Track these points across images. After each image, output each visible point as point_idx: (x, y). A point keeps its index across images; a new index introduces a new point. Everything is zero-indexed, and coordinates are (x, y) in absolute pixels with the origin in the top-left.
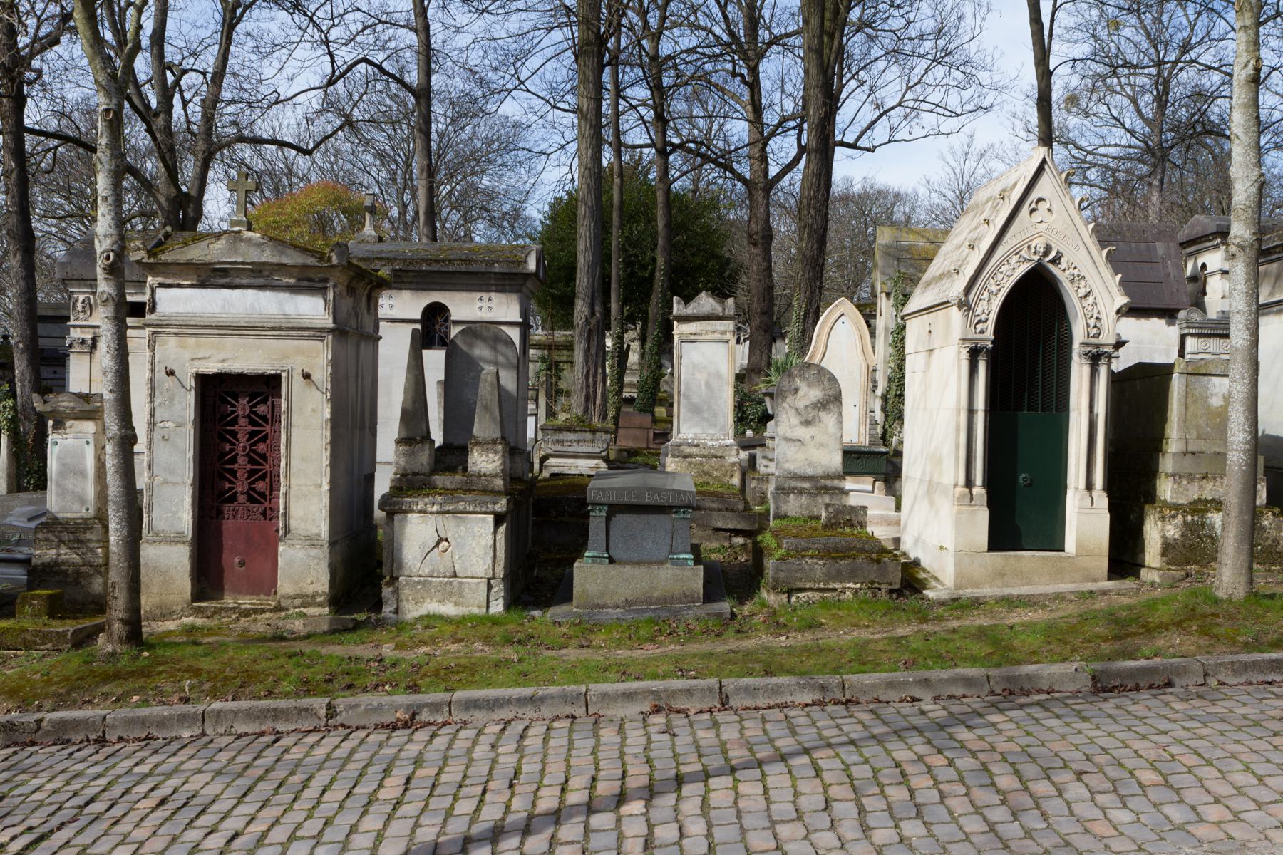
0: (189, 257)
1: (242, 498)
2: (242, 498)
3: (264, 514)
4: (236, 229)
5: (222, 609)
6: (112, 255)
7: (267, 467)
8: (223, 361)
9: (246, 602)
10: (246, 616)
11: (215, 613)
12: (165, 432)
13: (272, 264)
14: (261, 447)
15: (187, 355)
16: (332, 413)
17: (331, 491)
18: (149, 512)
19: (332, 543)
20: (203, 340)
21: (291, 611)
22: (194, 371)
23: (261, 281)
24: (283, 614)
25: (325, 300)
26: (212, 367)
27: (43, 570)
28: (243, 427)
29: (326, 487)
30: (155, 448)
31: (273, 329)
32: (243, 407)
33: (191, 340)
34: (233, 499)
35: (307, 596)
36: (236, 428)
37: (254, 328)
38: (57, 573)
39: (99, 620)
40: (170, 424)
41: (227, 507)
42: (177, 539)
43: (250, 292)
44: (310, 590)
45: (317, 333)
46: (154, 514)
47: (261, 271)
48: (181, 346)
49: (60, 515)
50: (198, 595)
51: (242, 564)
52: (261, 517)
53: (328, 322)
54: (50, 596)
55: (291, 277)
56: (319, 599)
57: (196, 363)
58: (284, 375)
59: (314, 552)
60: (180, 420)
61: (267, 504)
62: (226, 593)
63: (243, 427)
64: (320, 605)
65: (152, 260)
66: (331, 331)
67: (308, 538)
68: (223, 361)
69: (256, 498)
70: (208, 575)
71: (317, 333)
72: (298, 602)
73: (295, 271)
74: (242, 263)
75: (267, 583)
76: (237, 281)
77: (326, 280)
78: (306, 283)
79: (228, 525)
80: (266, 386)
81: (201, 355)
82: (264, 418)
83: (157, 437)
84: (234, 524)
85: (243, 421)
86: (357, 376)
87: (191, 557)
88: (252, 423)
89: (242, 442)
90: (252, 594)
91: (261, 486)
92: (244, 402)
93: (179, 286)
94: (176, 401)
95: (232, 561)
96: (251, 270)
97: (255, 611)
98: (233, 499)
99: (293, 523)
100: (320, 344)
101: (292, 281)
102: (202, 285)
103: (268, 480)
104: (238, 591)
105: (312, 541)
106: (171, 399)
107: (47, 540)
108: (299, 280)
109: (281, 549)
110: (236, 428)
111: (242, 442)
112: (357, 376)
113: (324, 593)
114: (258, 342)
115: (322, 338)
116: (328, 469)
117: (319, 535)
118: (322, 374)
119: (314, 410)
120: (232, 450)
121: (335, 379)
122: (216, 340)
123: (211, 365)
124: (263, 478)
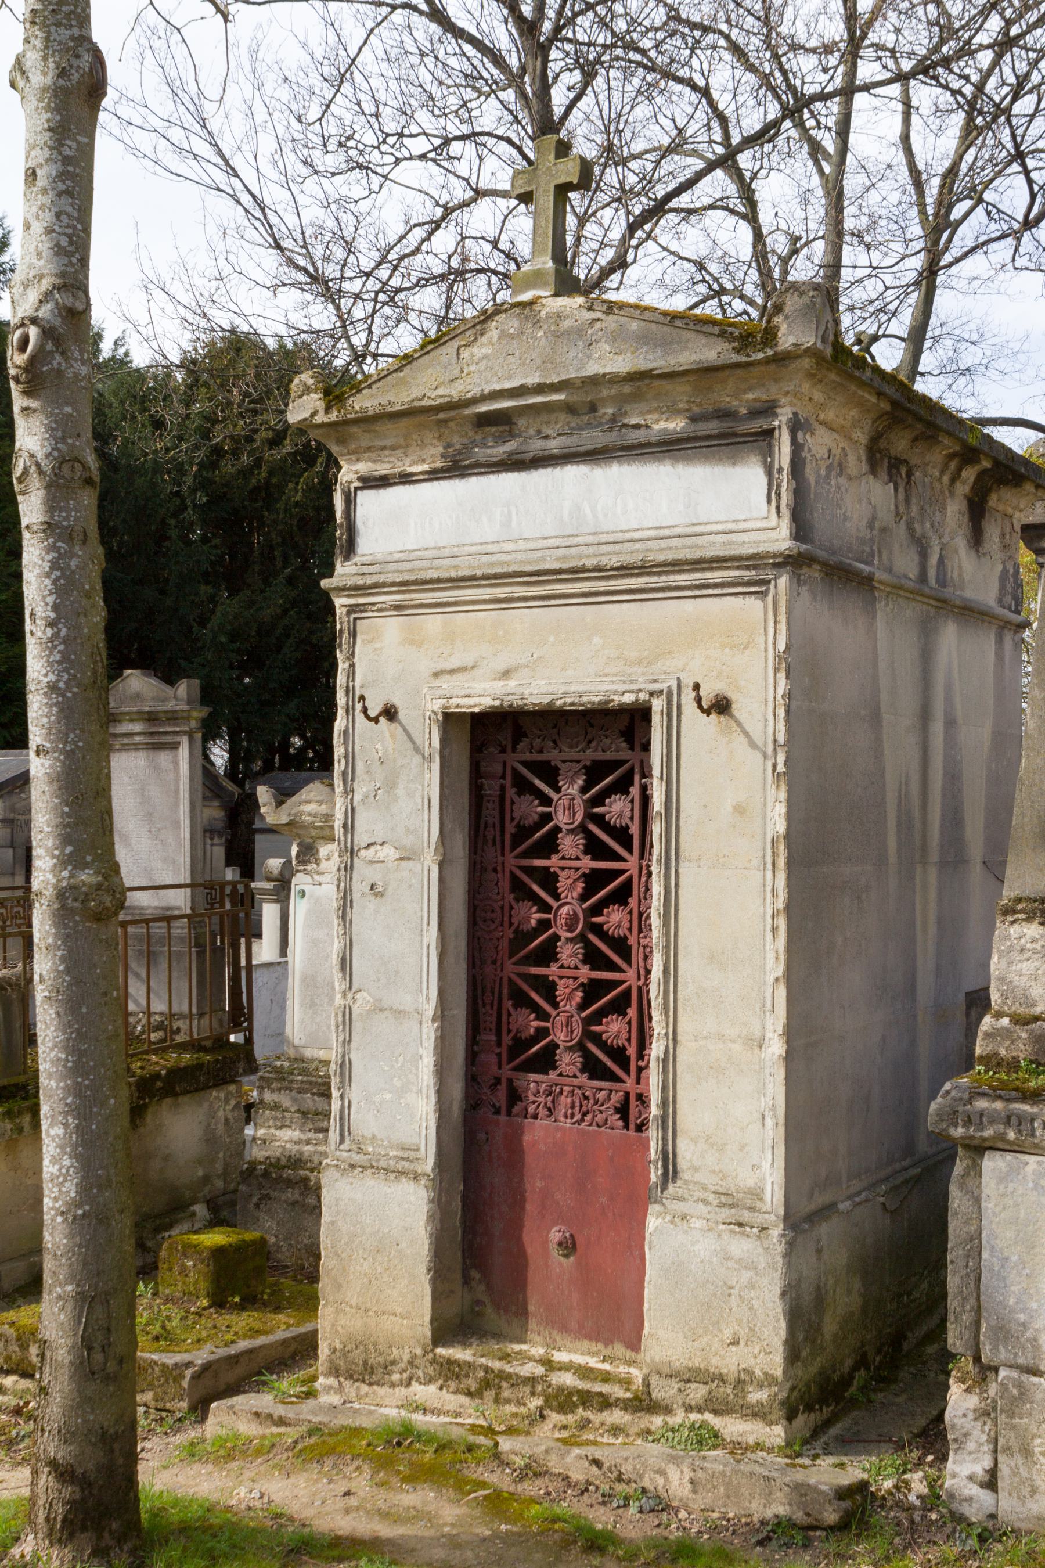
0: (416, 393)
1: (568, 1062)
2: (568, 1062)
3: (623, 1111)
4: (526, 296)
5: (503, 1376)
6: (33, 332)
7: (630, 976)
8: (506, 674)
9: (574, 1353)
10: (562, 1409)
11: (486, 1384)
12: (378, 878)
13: (614, 379)
14: (615, 918)
15: (426, 665)
16: (789, 817)
17: (789, 1058)
18: (341, 1087)
19: (799, 1222)
20: (460, 620)
21: (678, 1418)
22: (437, 705)
23: (597, 438)
24: (657, 1421)
25: (769, 471)
26: (480, 694)
27: (266, 1174)
28: (571, 860)
29: (777, 1047)
30: (356, 915)
31: (625, 570)
32: (568, 802)
33: (433, 623)
34: (546, 1061)
35: (722, 1379)
36: (553, 862)
37: (577, 572)
38: (289, 1183)
39: (282, 1327)
40: (388, 853)
41: (535, 1083)
42: (399, 1172)
43: (572, 472)
44: (730, 1362)
45: (750, 572)
46: (355, 1093)
47: (593, 408)
48: (413, 641)
49: (308, 1053)
50: (449, 1328)
51: (569, 1246)
52: (615, 1119)
53: (779, 538)
54: (219, 1253)
55: (673, 412)
56: (757, 1396)
57: (446, 684)
58: (658, 705)
59: (741, 1246)
60: (408, 841)
61: (629, 1084)
62: (532, 1324)
63: (571, 860)
64: (757, 1413)
65: (333, 416)
66: (790, 562)
67: (728, 1200)
68: (506, 674)
69: (615, 1062)
70: (482, 1268)
71: (750, 572)
72: (697, 1392)
73: (681, 391)
74: (540, 389)
75: (618, 1318)
76: (537, 445)
77: (768, 409)
78: (712, 427)
79: (540, 1134)
80: (613, 739)
81: (454, 663)
82: (622, 835)
83: (359, 888)
84: (552, 1130)
85: (570, 844)
86: (925, 715)
87: (431, 1218)
88: (594, 848)
89: (570, 902)
90: (594, 1336)
91: (614, 1028)
92: (572, 788)
93: (406, 479)
94: (400, 791)
95: (544, 1241)
96: (570, 409)
97: (586, 1399)
98: (546, 1061)
99: (686, 1152)
100: (754, 605)
101: (676, 425)
102: (455, 468)
103: (632, 1012)
104: (560, 1325)
105: (735, 1208)
106: (391, 785)
107: (276, 1107)
108: (693, 419)
109: (652, 1223)
110: (553, 862)
111: (570, 902)
112: (925, 715)
113: (770, 1380)
114: (590, 613)
115: (759, 588)
116: (782, 992)
117: (757, 1194)
118: (761, 698)
119: (740, 810)
120: (544, 925)
121: (795, 711)
122: (487, 617)
123: (478, 687)
124: (619, 1006)
